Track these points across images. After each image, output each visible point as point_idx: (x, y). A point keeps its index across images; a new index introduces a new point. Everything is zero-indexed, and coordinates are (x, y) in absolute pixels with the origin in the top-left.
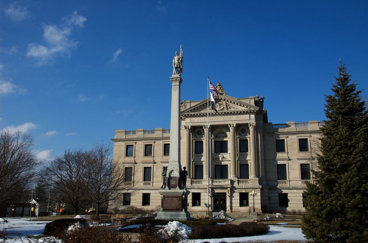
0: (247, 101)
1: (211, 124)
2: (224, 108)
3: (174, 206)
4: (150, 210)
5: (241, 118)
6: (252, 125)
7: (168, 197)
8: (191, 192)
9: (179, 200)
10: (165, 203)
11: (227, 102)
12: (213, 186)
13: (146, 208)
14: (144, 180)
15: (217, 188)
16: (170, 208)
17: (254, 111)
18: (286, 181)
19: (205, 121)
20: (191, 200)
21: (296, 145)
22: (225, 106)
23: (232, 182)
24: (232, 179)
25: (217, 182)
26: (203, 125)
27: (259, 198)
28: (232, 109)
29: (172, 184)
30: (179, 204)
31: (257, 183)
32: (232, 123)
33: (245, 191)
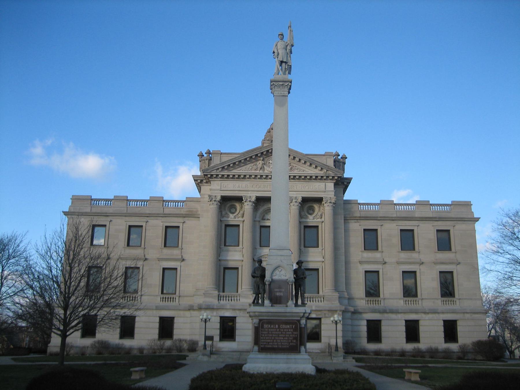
7: (270, 322)
9: (295, 330)
10: (263, 335)
13: (127, 343)
19: (246, 189)
21: (396, 240)
29: (278, 294)
30: (295, 338)
32: (295, 196)
33: (317, 315)
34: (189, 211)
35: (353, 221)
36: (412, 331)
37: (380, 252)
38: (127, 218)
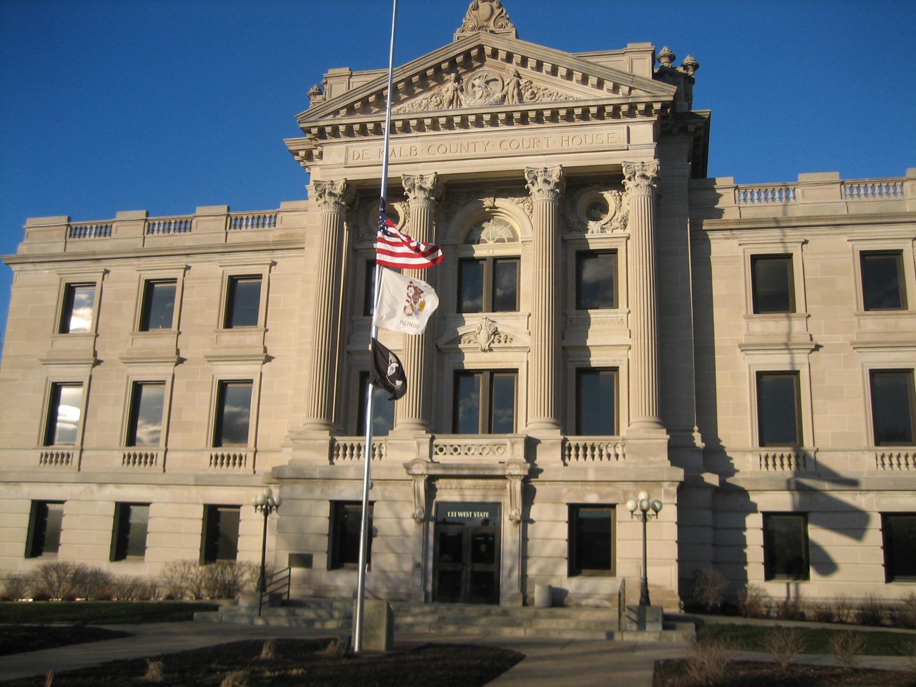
0: (619, 62)
1: (566, 164)
2: (504, 96)
5: (589, 140)
8: (760, 508)
11: (521, 70)
12: (435, 468)
13: (126, 571)
15: (457, 475)
19: (413, 158)
21: (851, 282)
22: (512, 85)
23: (531, 445)
24: (530, 435)
25: (456, 450)
26: (400, 174)
27: (671, 532)
31: (659, 459)
33: (601, 495)
34: (287, 235)
35: (719, 234)
36: (127, 537)
37: (800, 317)
38: (142, 262)
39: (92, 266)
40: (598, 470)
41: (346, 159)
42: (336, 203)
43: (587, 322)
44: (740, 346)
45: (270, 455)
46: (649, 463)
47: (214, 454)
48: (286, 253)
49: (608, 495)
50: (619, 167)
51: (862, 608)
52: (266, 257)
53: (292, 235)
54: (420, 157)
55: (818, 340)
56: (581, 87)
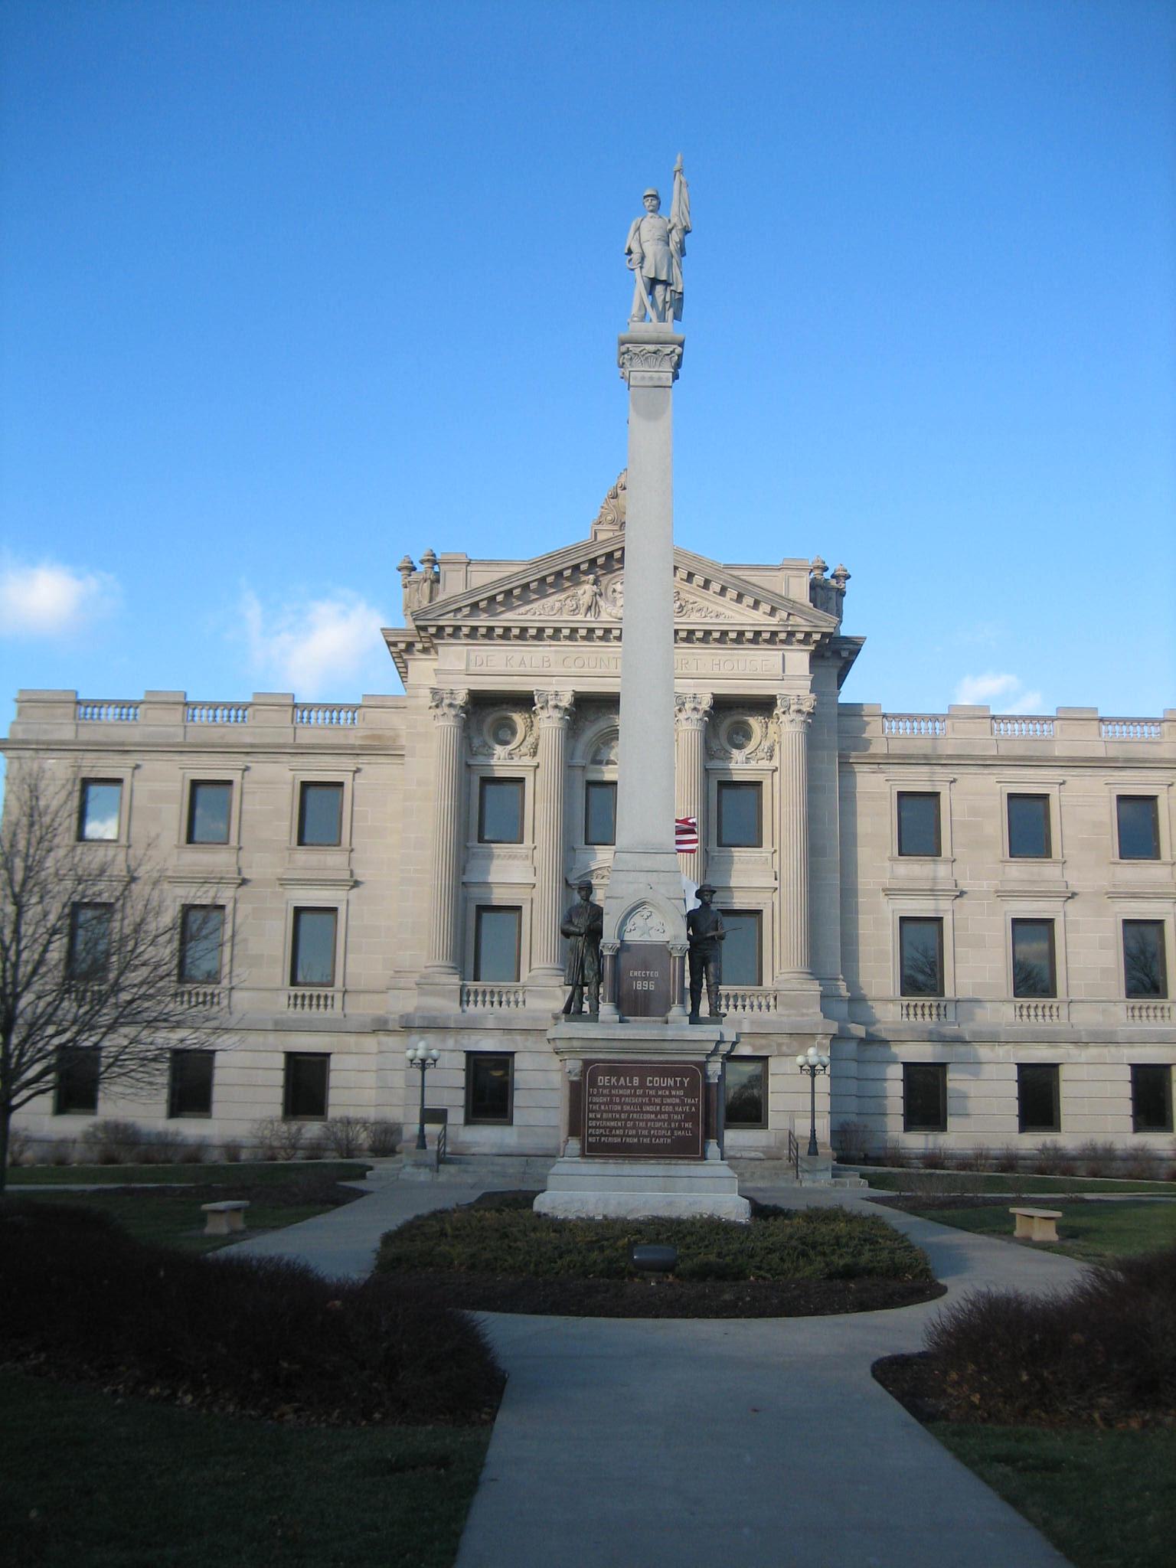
3: (658, 1125)
4: (191, 1140)
6: (551, 703)
7: (615, 1069)
9: (691, 1091)
10: (596, 1107)
13: (190, 1129)
14: (294, 982)
16: (628, 1140)
17: (808, 635)
18: (943, 1004)
19: (546, 671)
20: (462, 1094)
21: (997, 826)
28: (695, 617)
30: (691, 1117)
32: (693, 691)
33: (753, 1046)
35: (865, 768)
37: (946, 861)
38: (184, 757)
39: (116, 759)
40: (752, 1023)
41: (468, 665)
42: (456, 716)
43: (730, 860)
44: (884, 890)
45: (362, 997)
46: (803, 1015)
47: (292, 994)
48: (373, 759)
49: (762, 1047)
50: (774, 697)
51: (376, 1123)
52: (350, 763)
53: (379, 737)
54: (554, 670)
55: (964, 885)
56: (735, 606)
